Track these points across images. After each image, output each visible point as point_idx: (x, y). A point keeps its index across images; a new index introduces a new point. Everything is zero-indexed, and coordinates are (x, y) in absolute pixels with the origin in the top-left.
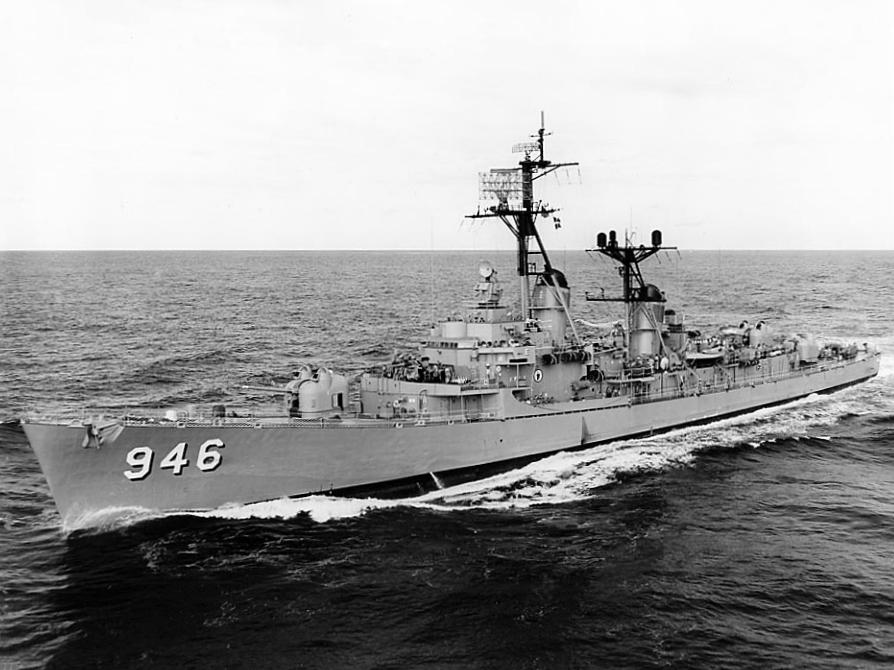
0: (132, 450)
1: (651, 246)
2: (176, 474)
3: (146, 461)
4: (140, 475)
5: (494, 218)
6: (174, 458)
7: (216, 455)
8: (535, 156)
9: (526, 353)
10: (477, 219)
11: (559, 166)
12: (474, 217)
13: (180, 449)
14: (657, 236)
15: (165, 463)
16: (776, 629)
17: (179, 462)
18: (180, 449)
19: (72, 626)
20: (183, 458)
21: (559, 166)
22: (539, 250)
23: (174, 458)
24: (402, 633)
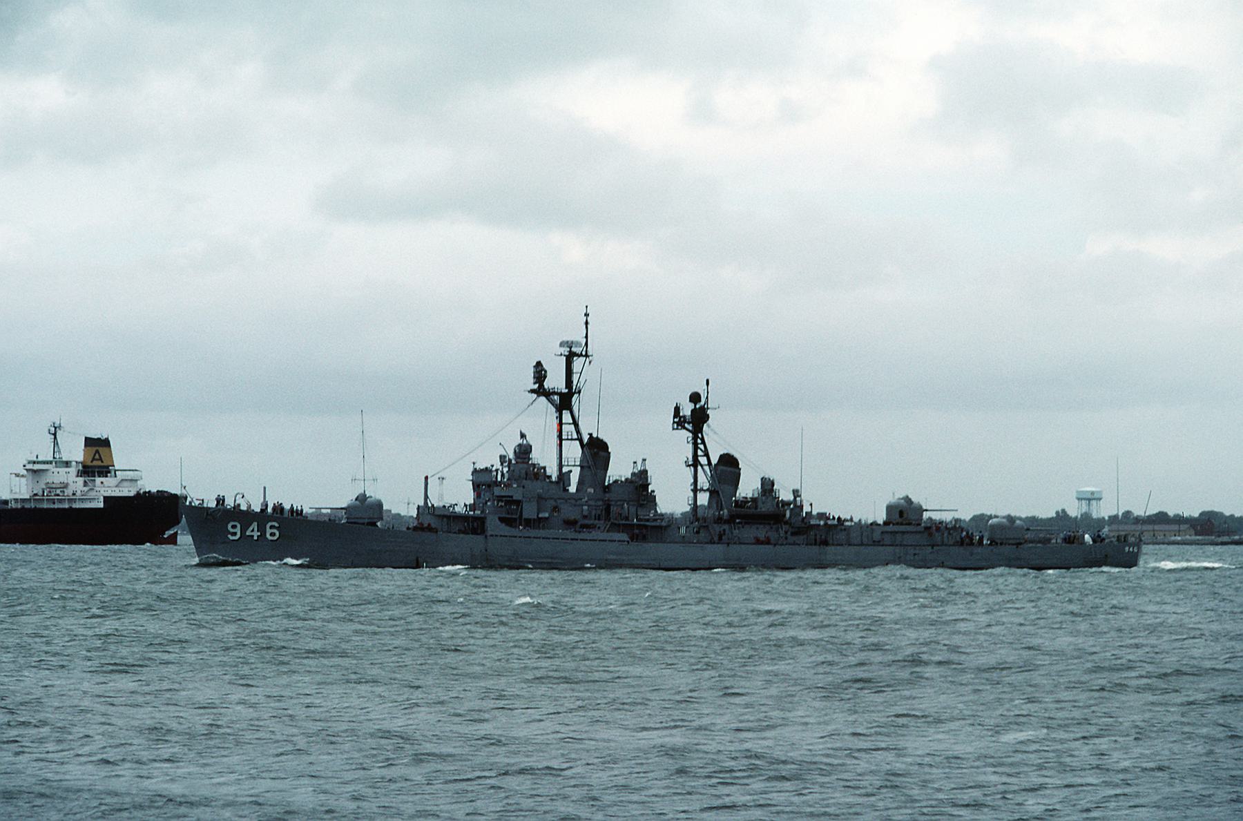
6: (253, 531)
17: (256, 534)
23: (253, 531)
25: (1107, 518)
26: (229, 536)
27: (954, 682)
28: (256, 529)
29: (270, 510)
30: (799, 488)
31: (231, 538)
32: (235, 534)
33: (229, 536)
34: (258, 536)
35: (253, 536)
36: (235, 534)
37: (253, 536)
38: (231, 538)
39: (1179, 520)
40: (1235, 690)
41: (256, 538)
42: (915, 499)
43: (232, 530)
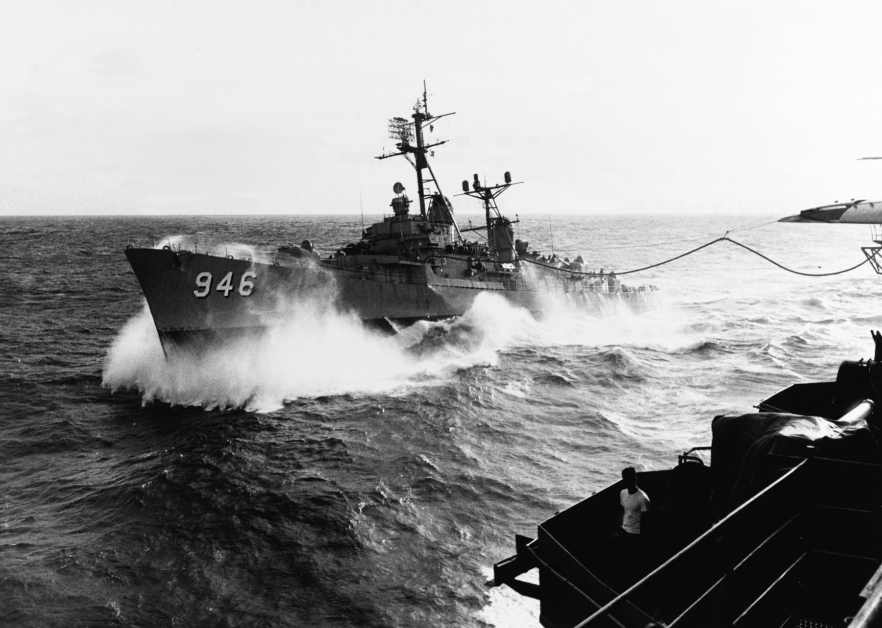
0: (196, 278)
1: (505, 183)
2: (226, 297)
3: (207, 284)
4: (203, 294)
5: (401, 156)
6: (225, 284)
7: (251, 285)
8: (422, 111)
9: (437, 240)
10: (383, 160)
11: (440, 117)
12: (380, 158)
13: (229, 276)
14: (507, 177)
15: (219, 287)
16: (590, 420)
17: (228, 288)
18: (229, 276)
19: (226, 240)
20: (231, 285)
21: (440, 117)
22: (432, 178)
23: (225, 284)
24: (18, 368)
25: (148, 396)
26: (196, 292)
27: (81, 366)
28: (229, 282)
29: (366, 232)
30: (536, 527)
31: (197, 294)
32: (202, 289)
33: (196, 292)
34: (230, 291)
35: (224, 291)
36: (202, 289)
37: (224, 291)
38: (197, 294)
39: (339, 396)
40: (880, 292)
41: (226, 294)
42: (390, 203)
43: (199, 283)
